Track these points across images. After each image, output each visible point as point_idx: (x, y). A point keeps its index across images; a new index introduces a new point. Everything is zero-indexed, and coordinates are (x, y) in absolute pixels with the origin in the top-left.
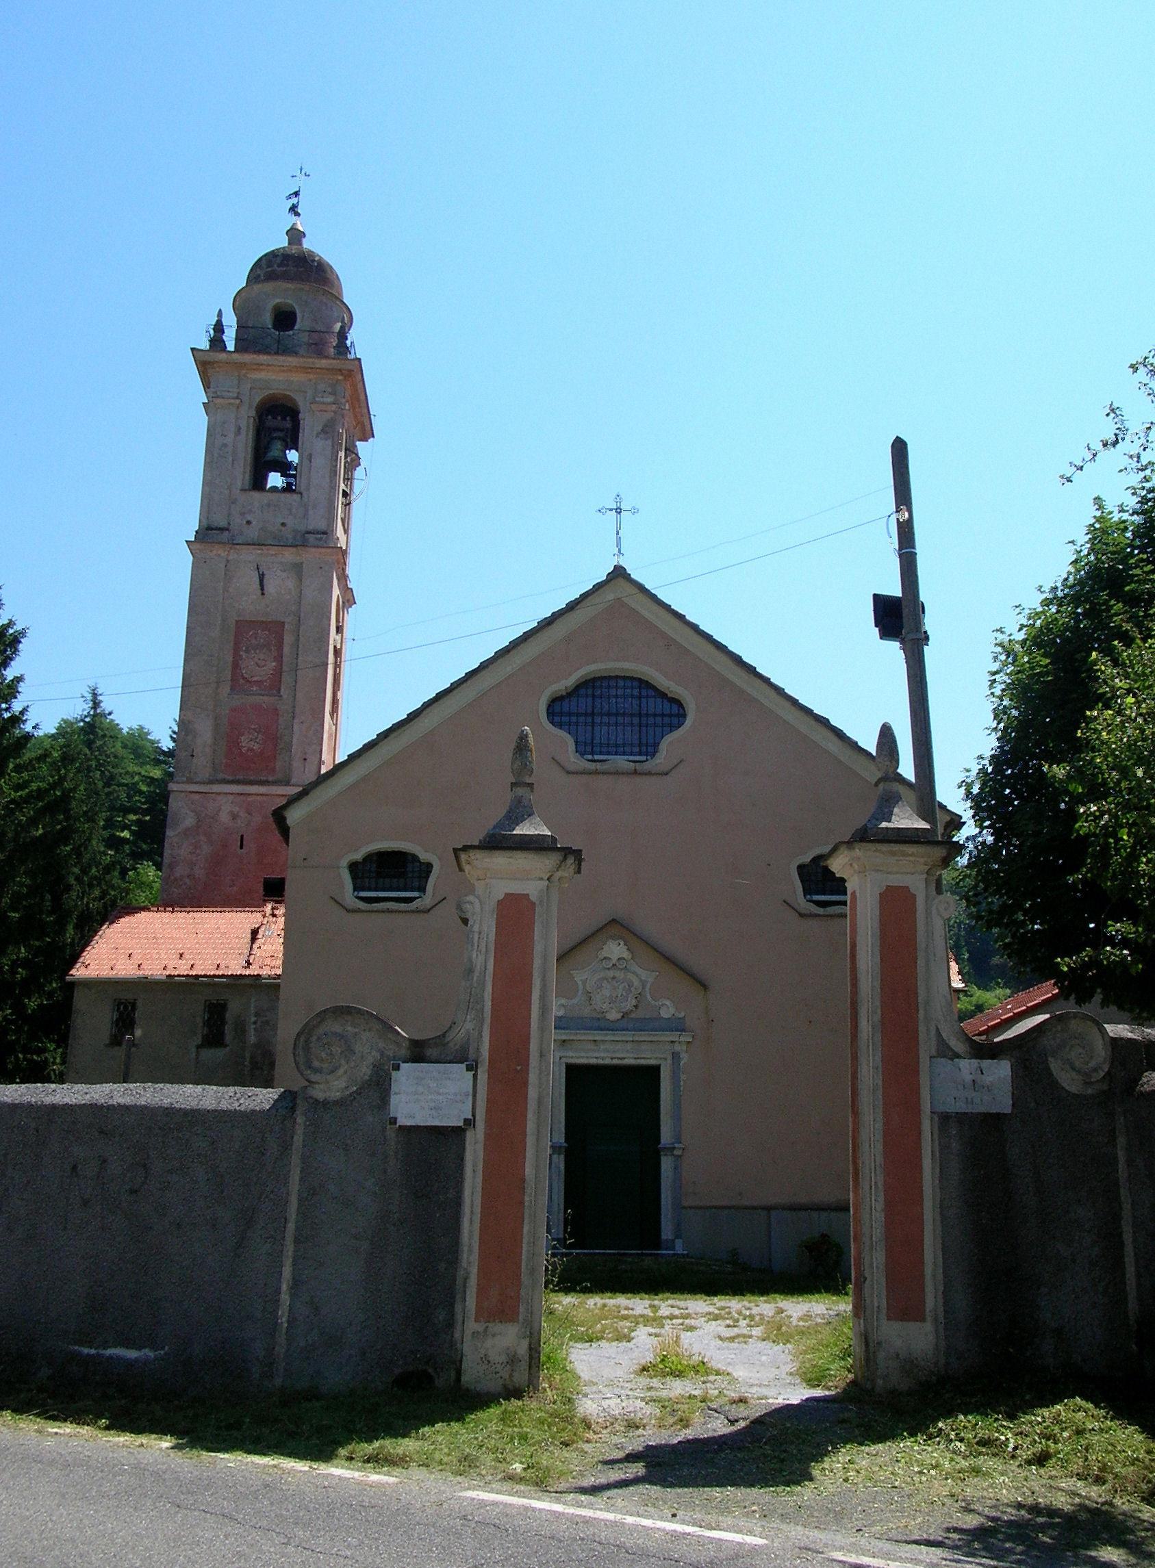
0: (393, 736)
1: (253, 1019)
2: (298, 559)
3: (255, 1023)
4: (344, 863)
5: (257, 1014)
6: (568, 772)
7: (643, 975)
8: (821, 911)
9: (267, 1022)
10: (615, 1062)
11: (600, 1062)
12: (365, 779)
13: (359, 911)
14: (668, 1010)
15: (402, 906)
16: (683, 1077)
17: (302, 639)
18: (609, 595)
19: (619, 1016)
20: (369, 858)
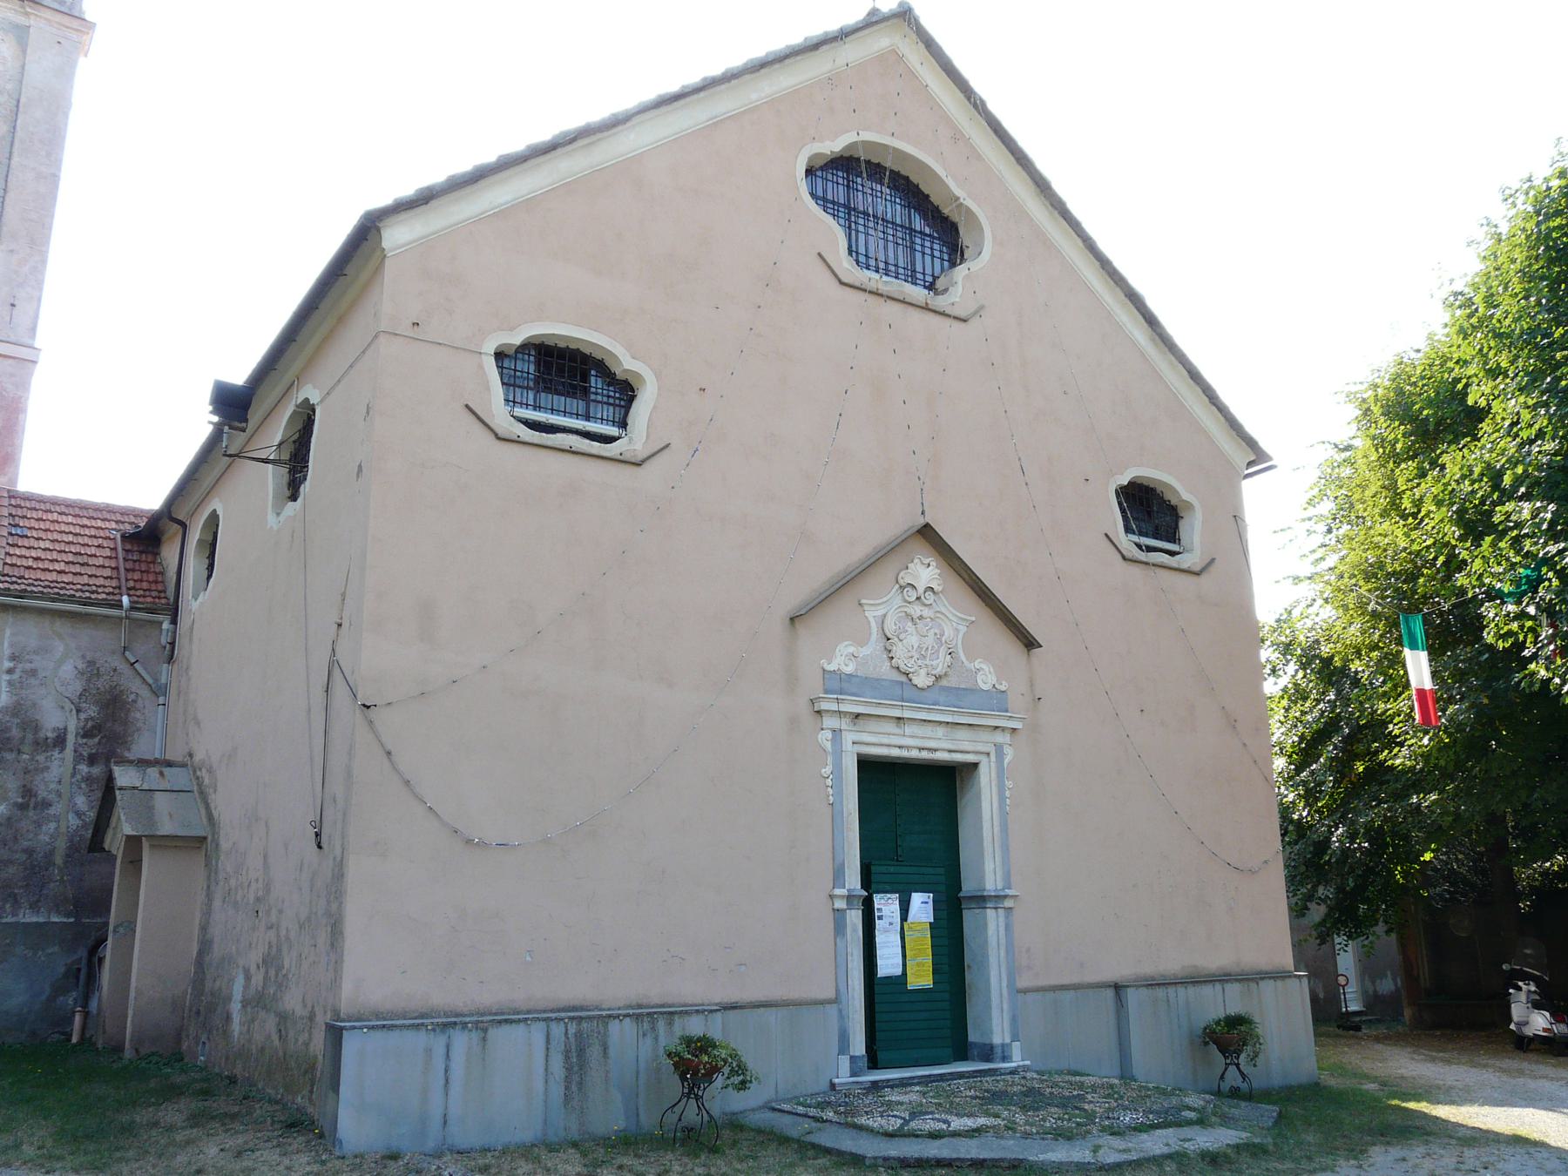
0: (825, 47)
1: (7, 664)
2: (21, 20)
3: (10, 671)
4: (490, 347)
5: (13, 658)
6: (841, 283)
7: (956, 618)
8: (1142, 556)
9: (33, 673)
10: (925, 755)
11: (905, 754)
12: (529, 204)
13: (518, 442)
14: (987, 679)
15: (596, 448)
16: (1009, 784)
17: (19, 134)
18: (881, 41)
19: (930, 681)
20: (525, 347)
